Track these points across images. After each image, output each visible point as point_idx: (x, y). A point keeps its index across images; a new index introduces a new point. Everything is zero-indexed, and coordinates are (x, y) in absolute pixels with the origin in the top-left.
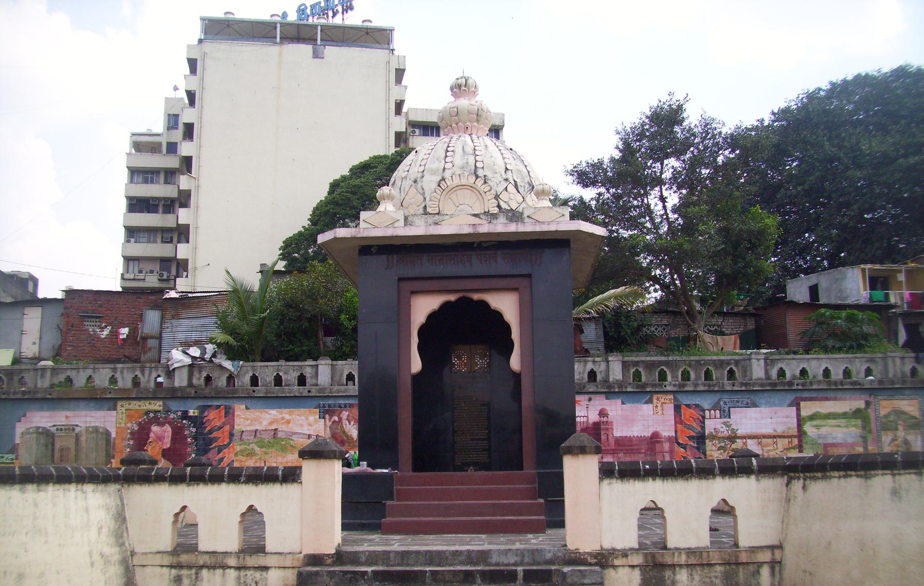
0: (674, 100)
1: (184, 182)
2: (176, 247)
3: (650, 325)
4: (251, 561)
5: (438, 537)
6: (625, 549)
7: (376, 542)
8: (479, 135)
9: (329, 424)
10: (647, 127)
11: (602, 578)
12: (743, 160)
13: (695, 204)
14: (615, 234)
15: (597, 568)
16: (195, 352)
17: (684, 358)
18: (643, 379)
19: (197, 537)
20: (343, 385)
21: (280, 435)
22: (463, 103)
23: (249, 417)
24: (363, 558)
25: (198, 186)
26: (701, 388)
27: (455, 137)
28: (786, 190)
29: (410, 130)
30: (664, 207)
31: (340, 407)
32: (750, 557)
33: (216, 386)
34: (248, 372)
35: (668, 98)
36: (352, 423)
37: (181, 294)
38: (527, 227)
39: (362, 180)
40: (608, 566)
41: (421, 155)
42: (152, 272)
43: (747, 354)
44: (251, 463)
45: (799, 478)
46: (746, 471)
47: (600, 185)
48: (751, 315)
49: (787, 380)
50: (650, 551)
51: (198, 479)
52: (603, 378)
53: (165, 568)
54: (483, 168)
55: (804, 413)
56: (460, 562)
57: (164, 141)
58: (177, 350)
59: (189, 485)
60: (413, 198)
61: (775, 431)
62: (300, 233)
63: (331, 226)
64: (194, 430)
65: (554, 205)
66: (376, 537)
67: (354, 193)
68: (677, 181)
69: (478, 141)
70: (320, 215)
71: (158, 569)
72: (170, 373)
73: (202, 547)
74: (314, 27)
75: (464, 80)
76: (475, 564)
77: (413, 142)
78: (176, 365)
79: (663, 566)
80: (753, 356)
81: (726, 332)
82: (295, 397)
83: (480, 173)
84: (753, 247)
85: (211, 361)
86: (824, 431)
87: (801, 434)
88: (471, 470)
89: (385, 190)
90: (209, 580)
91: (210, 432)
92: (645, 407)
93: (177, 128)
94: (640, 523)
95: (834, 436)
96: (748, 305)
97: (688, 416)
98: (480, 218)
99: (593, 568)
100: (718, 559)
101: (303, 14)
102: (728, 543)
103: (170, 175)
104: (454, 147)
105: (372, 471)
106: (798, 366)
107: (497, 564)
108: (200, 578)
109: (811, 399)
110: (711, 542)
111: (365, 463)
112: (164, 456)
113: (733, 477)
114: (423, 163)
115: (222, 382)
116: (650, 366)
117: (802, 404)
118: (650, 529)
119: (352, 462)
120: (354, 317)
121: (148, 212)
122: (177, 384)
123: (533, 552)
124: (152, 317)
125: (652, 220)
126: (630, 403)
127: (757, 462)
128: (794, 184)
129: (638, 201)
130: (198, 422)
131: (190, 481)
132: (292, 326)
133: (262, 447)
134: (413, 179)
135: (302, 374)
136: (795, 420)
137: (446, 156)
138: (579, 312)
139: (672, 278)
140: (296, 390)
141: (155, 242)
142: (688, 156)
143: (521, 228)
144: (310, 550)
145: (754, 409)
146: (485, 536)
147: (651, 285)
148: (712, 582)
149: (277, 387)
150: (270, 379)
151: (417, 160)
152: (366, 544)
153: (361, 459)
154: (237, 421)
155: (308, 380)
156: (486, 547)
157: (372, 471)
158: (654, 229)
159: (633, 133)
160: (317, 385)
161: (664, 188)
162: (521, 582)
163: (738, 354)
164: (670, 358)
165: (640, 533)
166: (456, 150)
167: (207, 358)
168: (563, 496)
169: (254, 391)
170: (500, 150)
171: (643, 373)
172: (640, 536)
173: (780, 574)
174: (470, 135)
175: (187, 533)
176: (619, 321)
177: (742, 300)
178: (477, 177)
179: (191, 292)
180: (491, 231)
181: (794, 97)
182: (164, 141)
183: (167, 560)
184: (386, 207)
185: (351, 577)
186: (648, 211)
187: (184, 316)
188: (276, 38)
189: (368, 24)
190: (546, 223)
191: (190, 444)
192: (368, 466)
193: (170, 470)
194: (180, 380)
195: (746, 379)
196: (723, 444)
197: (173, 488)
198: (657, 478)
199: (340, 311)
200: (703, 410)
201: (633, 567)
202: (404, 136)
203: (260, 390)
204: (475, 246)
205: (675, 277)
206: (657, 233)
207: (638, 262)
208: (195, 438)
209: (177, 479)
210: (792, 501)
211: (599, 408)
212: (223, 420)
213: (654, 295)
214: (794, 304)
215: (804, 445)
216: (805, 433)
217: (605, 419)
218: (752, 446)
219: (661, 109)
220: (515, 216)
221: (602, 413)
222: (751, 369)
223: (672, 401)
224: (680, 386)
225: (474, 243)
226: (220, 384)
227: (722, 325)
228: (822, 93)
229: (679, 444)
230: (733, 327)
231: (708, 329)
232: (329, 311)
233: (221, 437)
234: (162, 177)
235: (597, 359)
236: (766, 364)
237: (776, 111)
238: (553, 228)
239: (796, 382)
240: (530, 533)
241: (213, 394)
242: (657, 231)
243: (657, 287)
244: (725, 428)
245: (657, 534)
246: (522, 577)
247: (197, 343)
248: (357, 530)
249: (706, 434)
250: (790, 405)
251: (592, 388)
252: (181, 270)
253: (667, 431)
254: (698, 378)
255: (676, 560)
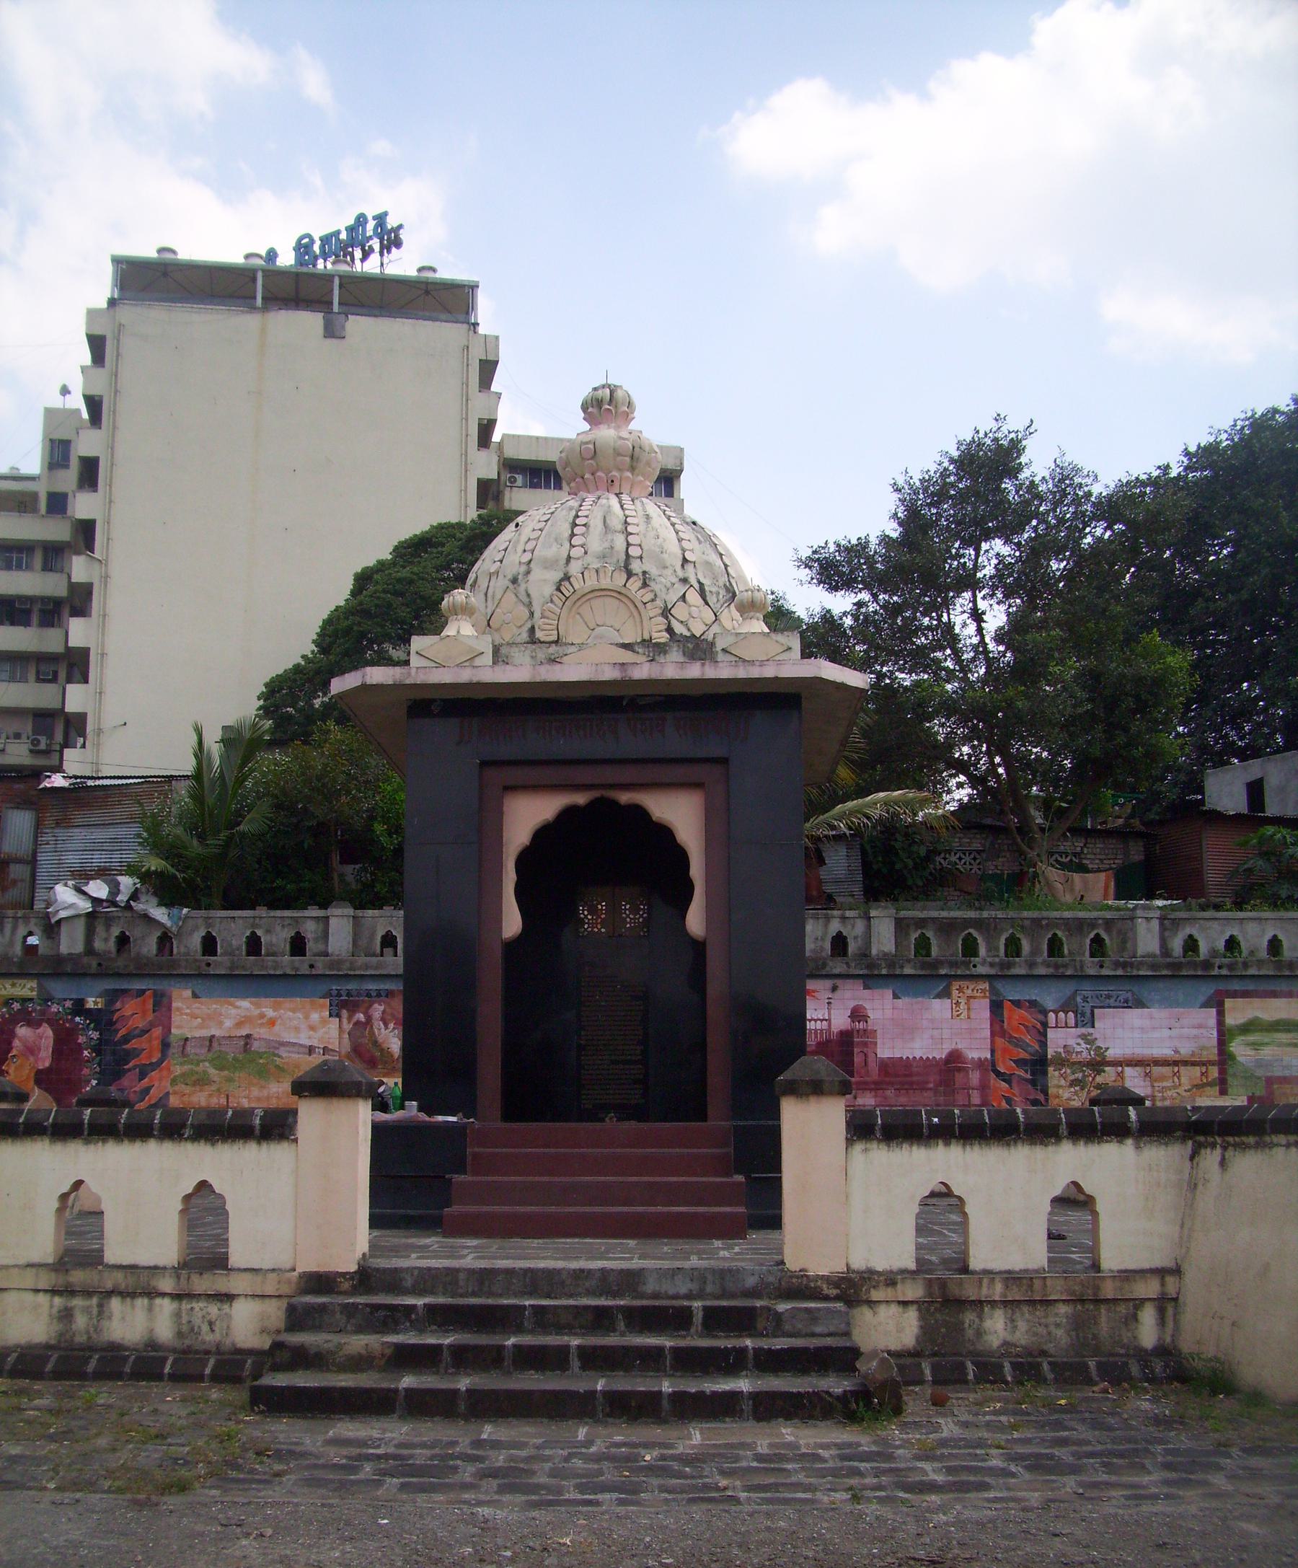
0: (1005, 430)
1: (80, 569)
2: (64, 689)
3: (949, 852)
4: (203, 1283)
5: (547, 1243)
6: (891, 1272)
7: (434, 1251)
8: (635, 494)
9: (347, 1026)
10: (952, 478)
11: (848, 1324)
12: (1125, 549)
13: (1042, 625)
14: (888, 681)
15: (839, 1305)
16: (99, 889)
17: (1011, 914)
18: (935, 951)
19: (101, 1237)
20: (374, 955)
21: (256, 1046)
22: (606, 433)
23: (197, 1012)
24: (409, 1282)
25: (107, 577)
26: (1041, 971)
27: (590, 499)
28: (1207, 601)
29: (506, 476)
30: (980, 631)
31: (369, 995)
32: (1121, 1289)
33: (138, 954)
34: (196, 928)
35: (994, 426)
36: (391, 1026)
37: (74, 781)
38: (723, 671)
39: (415, 569)
40: (859, 1301)
41: (526, 532)
42: (17, 736)
43: (1128, 909)
44: (201, 1099)
45: (1213, 1146)
46: (1117, 1131)
47: (860, 586)
48: (1138, 835)
49: (1202, 957)
50: (939, 1274)
51: (104, 1131)
52: (859, 949)
53: (41, 1294)
54: (641, 558)
55: (1230, 1020)
56: (587, 1290)
57: (42, 490)
58: (66, 885)
59: (87, 1142)
60: (512, 614)
61: (1176, 1052)
62: (297, 669)
63: (354, 660)
64: (95, 1035)
65: (773, 629)
66: (432, 1241)
67: (397, 594)
68: (1005, 583)
69: (633, 507)
70: (335, 635)
71: (29, 1297)
72: (52, 929)
73: (111, 1257)
74: (327, 278)
75: (608, 391)
76: (615, 1295)
77: (511, 499)
78: (63, 914)
79: (961, 1304)
80: (1139, 913)
81: (1090, 866)
82: (285, 976)
83: (636, 567)
84: (1142, 707)
85: (128, 907)
86: (1267, 1053)
87: (1224, 1058)
88: (611, 1118)
89: (458, 595)
90: (123, 1318)
91: (126, 1040)
92: (936, 1003)
93: (67, 467)
94: (921, 1221)
95: (1285, 1063)
96: (1132, 816)
97: (1015, 1023)
98: (634, 651)
99: (831, 1305)
100: (1061, 1293)
101: (307, 253)
102: (1081, 1263)
103: (53, 555)
104: (587, 517)
105: (427, 1119)
106: (1222, 932)
107: (656, 1296)
108: (107, 1314)
109: (1246, 994)
110: (1050, 1260)
111: (415, 1103)
112: (38, 1082)
113: (1093, 1142)
114: (530, 546)
115: (149, 946)
116: (948, 928)
117: (1228, 1003)
118: (940, 1233)
119: (390, 1102)
120: (396, 829)
121: (12, 624)
122: (64, 949)
123: (722, 1274)
124: (20, 822)
125: (957, 655)
126: (908, 995)
127: (1137, 1114)
128: (1223, 590)
129: (932, 618)
130: (103, 1020)
131: (89, 1135)
132: (281, 843)
133: (221, 1069)
134: (510, 576)
135: (298, 933)
136: (1215, 1033)
137: (573, 535)
138: (815, 825)
139: (992, 762)
140: (287, 962)
141: (24, 679)
142: (1026, 536)
143: (711, 672)
144: (309, 1264)
145: (1139, 1011)
146: (635, 1242)
147: (951, 776)
148: (1049, 1333)
149: (252, 958)
150: (240, 942)
151: (518, 541)
152: (414, 1256)
153: (406, 1096)
154: (176, 1019)
155: (311, 946)
156: (636, 1264)
157: (427, 1119)
158: (960, 671)
159: (925, 490)
160: (327, 955)
161: (979, 595)
162: (700, 1328)
163: (1110, 908)
164: (985, 914)
165: (920, 1240)
166: (592, 523)
167: (122, 901)
168: (780, 1171)
169: (209, 965)
170: (673, 525)
171: (934, 942)
172: (919, 1247)
173: (1176, 1321)
174: (617, 495)
175: (83, 1229)
176: (892, 843)
177: (1122, 806)
178: (630, 574)
179: (89, 778)
180: (654, 676)
181: (1226, 424)
182: (42, 490)
183: (46, 1280)
184: (461, 629)
185: (386, 1316)
186: (949, 637)
187: (79, 821)
188: (255, 298)
189: (430, 275)
190: (757, 663)
191: (88, 1061)
192: (420, 1109)
193: (53, 1114)
194: (72, 942)
195: (1125, 955)
196: (1079, 1075)
197: (59, 1147)
198: (953, 1141)
199: (372, 818)
200: (1045, 1012)
201: (905, 1304)
202: (493, 489)
203: (220, 962)
204: (624, 703)
205: (997, 760)
206: (965, 679)
207: (930, 734)
208: (98, 1049)
209: (65, 1131)
210: (1200, 1187)
211: (852, 1004)
212: (150, 1017)
213: (959, 793)
214: (1217, 817)
215: (1230, 1079)
216: (1232, 1057)
217: (861, 1026)
218: (1135, 1082)
219: (978, 445)
220: (699, 648)
221: (857, 1014)
222: (1135, 940)
223: (987, 994)
224: (1004, 966)
225: (622, 698)
226: (145, 951)
227: (1082, 852)
228: (1280, 418)
229: (998, 1074)
230: (1103, 857)
231: (1056, 860)
232: (352, 818)
233: (147, 1047)
234: (38, 559)
235: (848, 914)
236: (1163, 928)
237: (1193, 449)
238: (769, 672)
239: (1217, 961)
240: (718, 1238)
241: (132, 969)
242: (966, 675)
243: (962, 778)
244: (1084, 1046)
245: (950, 1243)
246: (700, 1321)
247: (103, 873)
248: (399, 1228)
249: (1049, 1057)
250: (1206, 1005)
251: (838, 967)
252: (73, 734)
253: (977, 1050)
254: (1036, 951)
255: (984, 1292)
